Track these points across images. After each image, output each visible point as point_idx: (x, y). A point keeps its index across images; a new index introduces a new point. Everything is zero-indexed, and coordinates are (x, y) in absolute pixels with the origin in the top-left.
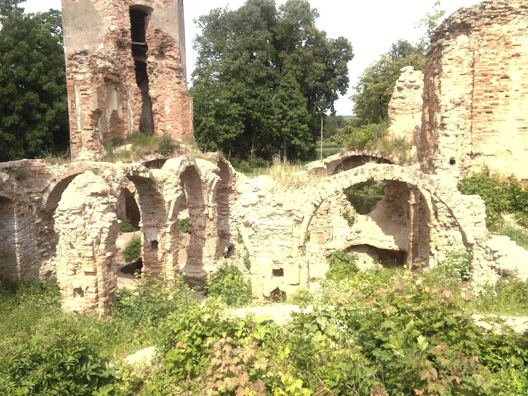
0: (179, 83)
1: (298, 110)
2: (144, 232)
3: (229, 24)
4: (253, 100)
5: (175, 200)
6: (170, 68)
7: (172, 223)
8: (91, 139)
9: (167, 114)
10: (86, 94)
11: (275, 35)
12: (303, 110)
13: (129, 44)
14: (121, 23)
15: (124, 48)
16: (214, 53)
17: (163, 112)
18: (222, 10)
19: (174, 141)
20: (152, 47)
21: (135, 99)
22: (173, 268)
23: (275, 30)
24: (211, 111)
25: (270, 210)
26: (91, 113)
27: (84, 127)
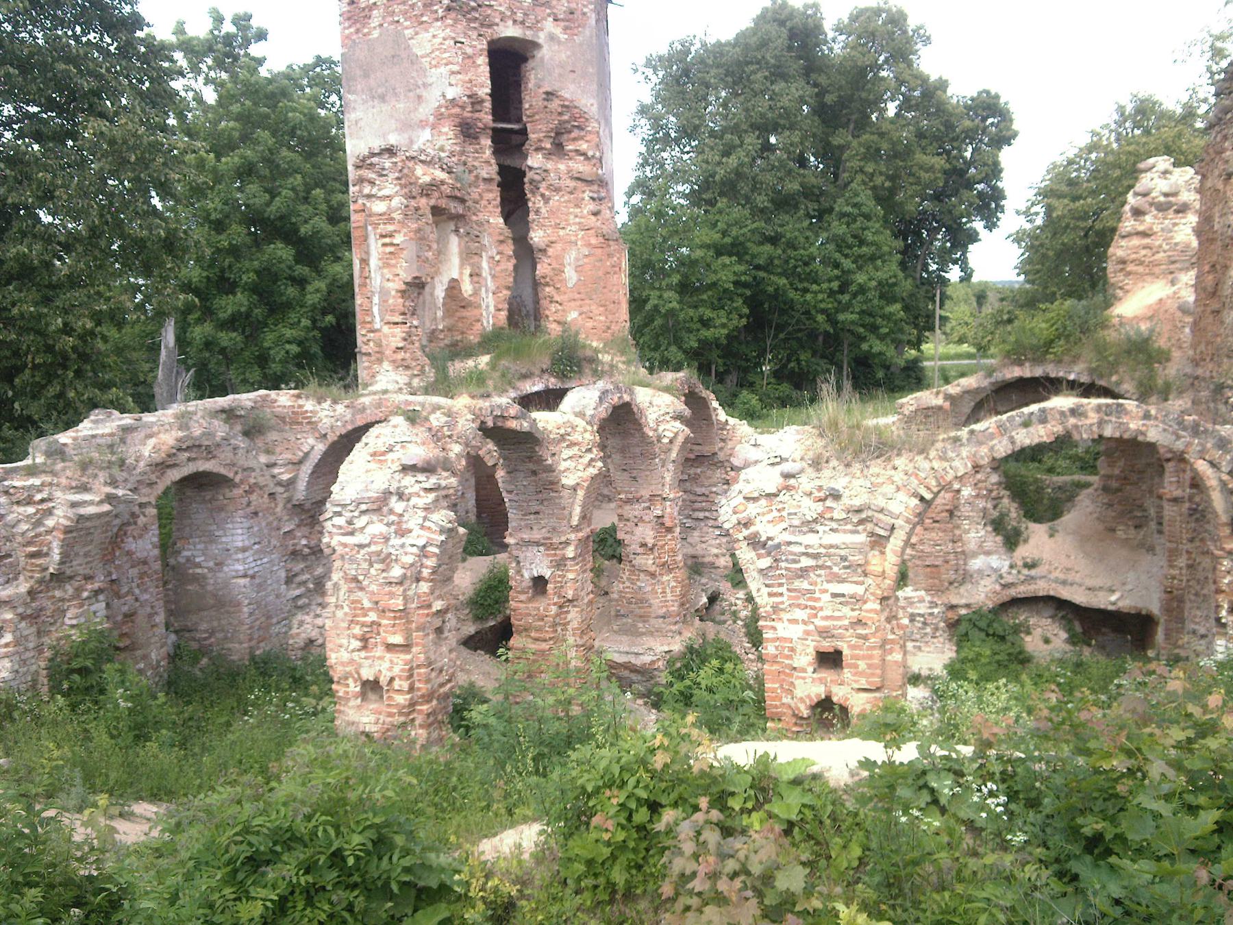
6: (578, 179)
8: (400, 345)
9: (570, 285)
10: (392, 244)
12: (890, 269)
14: (471, 81)
16: (677, 141)
20: (537, 132)
23: (823, 80)
25: (810, 509)
26: (403, 287)
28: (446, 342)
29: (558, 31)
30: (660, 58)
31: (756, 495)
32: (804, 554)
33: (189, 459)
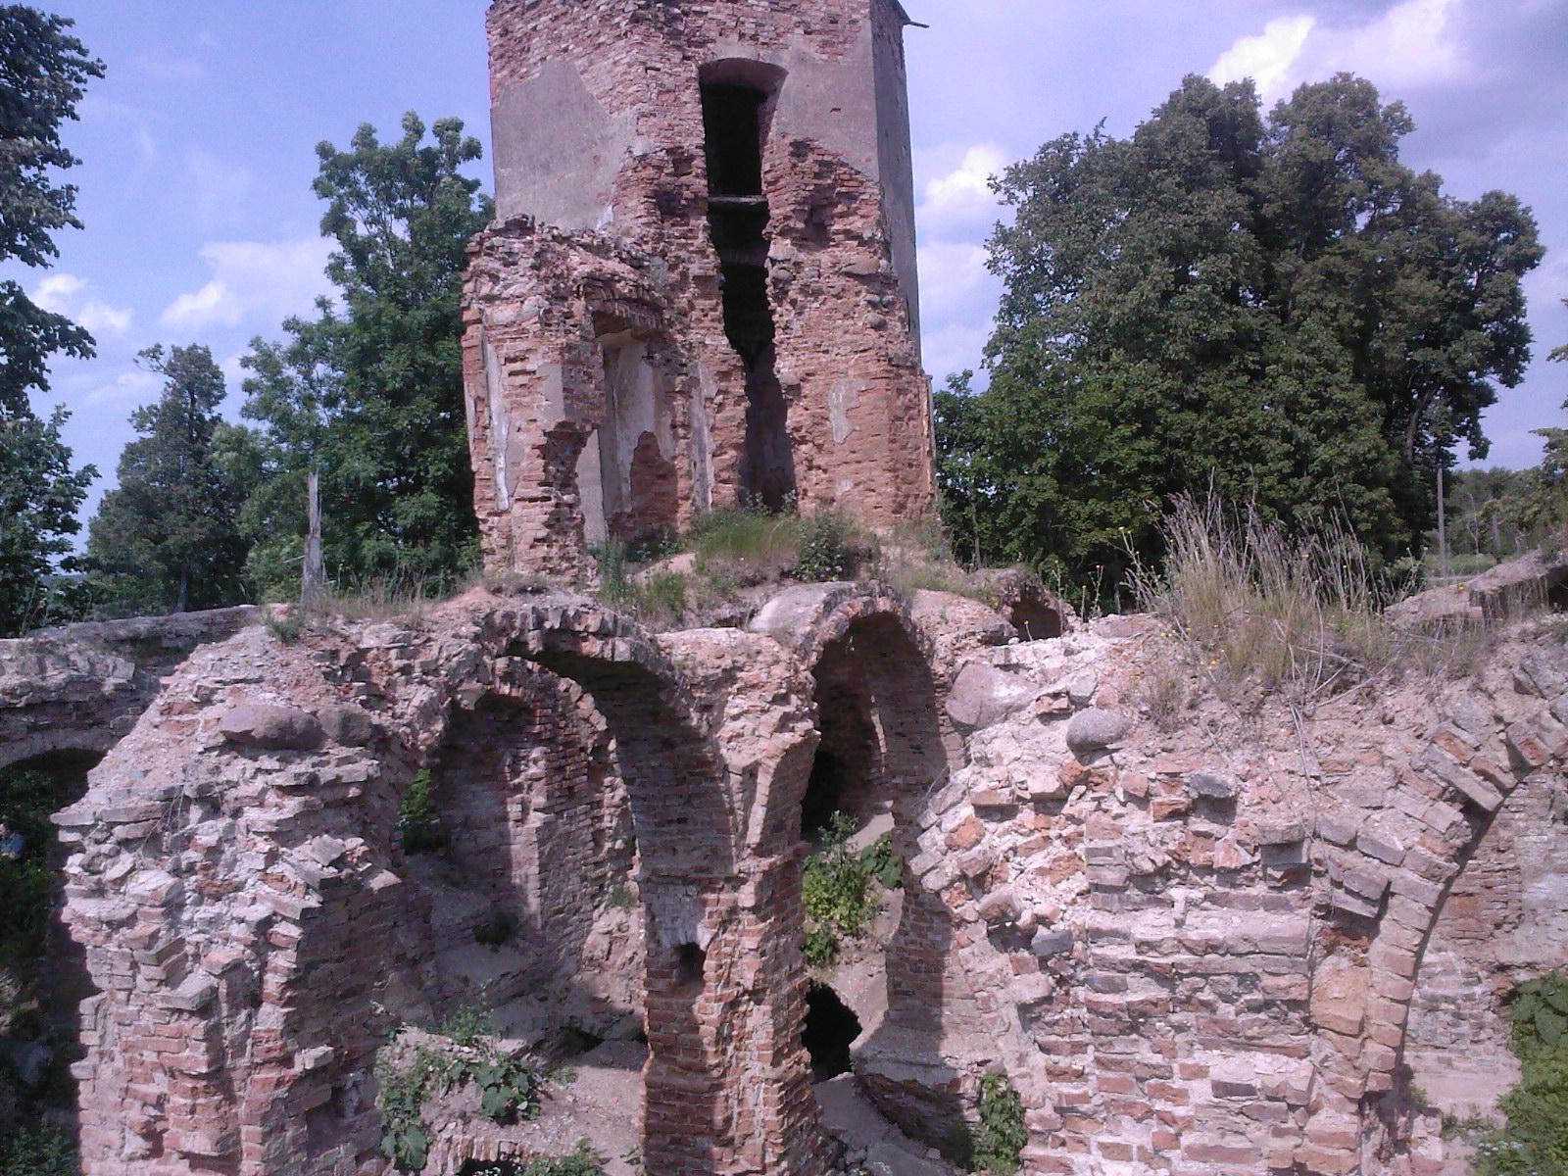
0: (879, 327)
1: (1351, 440)
2: (649, 907)
3: (1101, 180)
4: (1189, 416)
5: (773, 764)
6: (848, 274)
7: (765, 863)
8: (542, 533)
9: (838, 439)
10: (524, 372)
11: (1257, 201)
12: (1367, 439)
13: (697, 198)
14: (671, 127)
15: (683, 216)
16: (1056, 280)
17: (824, 434)
18: (1081, 140)
19: (855, 534)
20: (781, 204)
21: (719, 392)
22: (772, 1073)
23: (1260, 185)
24: (1043, 455)
25: (1145, 835)
26: (543, 440)
27: (521, 491)
28: (637, 533)
29: (812, 49)
30: (1029, 168)
31: (1004, 797)
32: (1137, 966)
33: (33, 728)
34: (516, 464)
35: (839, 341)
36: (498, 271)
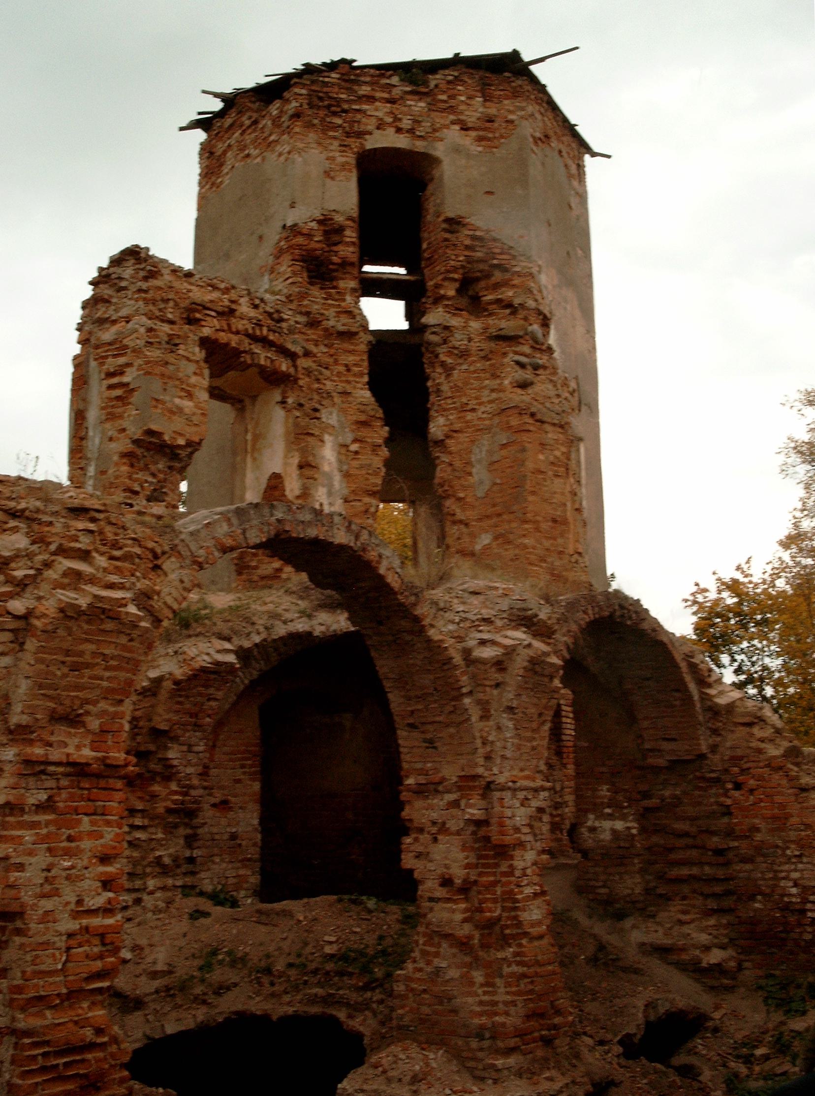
21: (355, 440)
26: (130, 447)
29: (467, 141)
34: (103, 473)
35: (485, 399)
36: (111, 296)
